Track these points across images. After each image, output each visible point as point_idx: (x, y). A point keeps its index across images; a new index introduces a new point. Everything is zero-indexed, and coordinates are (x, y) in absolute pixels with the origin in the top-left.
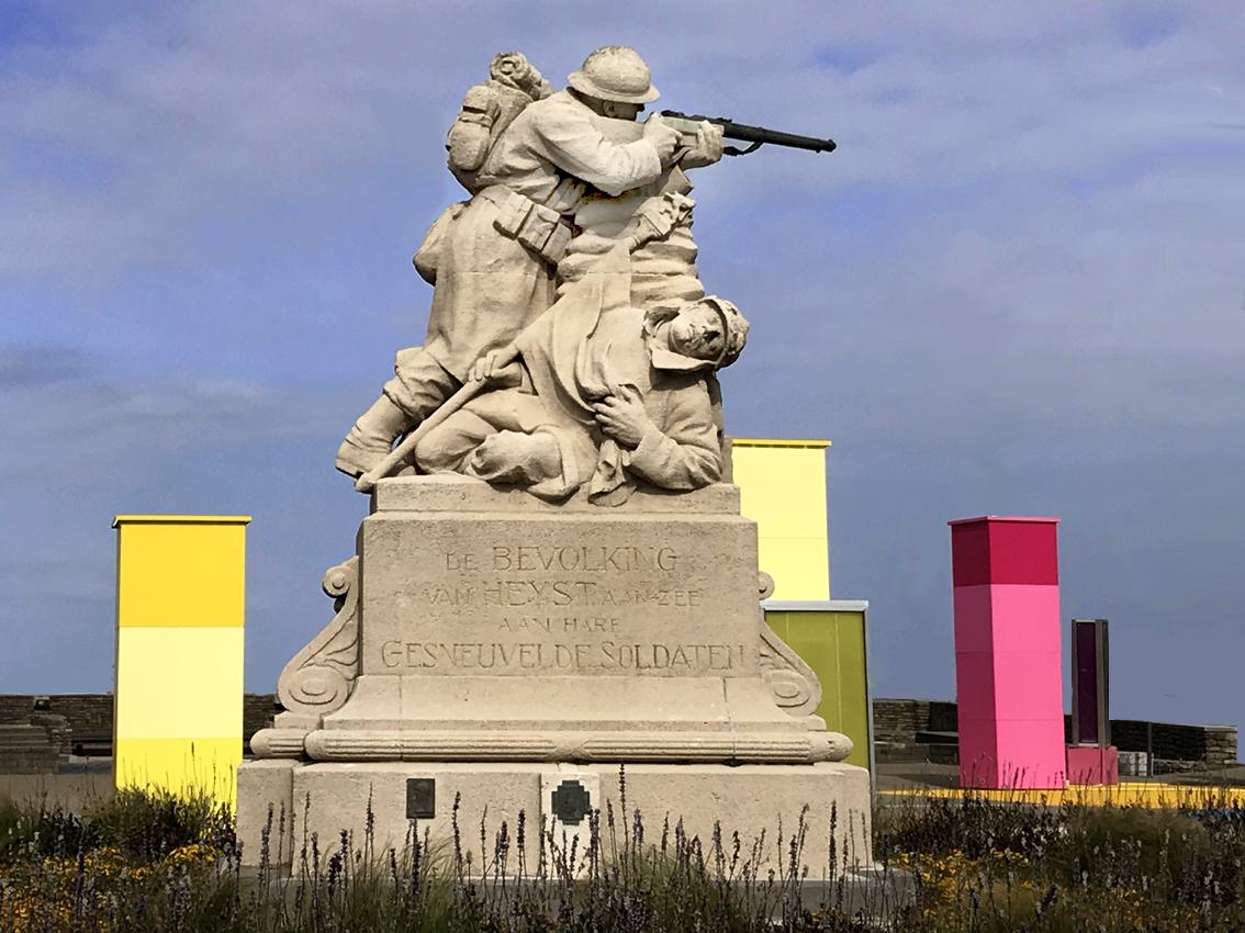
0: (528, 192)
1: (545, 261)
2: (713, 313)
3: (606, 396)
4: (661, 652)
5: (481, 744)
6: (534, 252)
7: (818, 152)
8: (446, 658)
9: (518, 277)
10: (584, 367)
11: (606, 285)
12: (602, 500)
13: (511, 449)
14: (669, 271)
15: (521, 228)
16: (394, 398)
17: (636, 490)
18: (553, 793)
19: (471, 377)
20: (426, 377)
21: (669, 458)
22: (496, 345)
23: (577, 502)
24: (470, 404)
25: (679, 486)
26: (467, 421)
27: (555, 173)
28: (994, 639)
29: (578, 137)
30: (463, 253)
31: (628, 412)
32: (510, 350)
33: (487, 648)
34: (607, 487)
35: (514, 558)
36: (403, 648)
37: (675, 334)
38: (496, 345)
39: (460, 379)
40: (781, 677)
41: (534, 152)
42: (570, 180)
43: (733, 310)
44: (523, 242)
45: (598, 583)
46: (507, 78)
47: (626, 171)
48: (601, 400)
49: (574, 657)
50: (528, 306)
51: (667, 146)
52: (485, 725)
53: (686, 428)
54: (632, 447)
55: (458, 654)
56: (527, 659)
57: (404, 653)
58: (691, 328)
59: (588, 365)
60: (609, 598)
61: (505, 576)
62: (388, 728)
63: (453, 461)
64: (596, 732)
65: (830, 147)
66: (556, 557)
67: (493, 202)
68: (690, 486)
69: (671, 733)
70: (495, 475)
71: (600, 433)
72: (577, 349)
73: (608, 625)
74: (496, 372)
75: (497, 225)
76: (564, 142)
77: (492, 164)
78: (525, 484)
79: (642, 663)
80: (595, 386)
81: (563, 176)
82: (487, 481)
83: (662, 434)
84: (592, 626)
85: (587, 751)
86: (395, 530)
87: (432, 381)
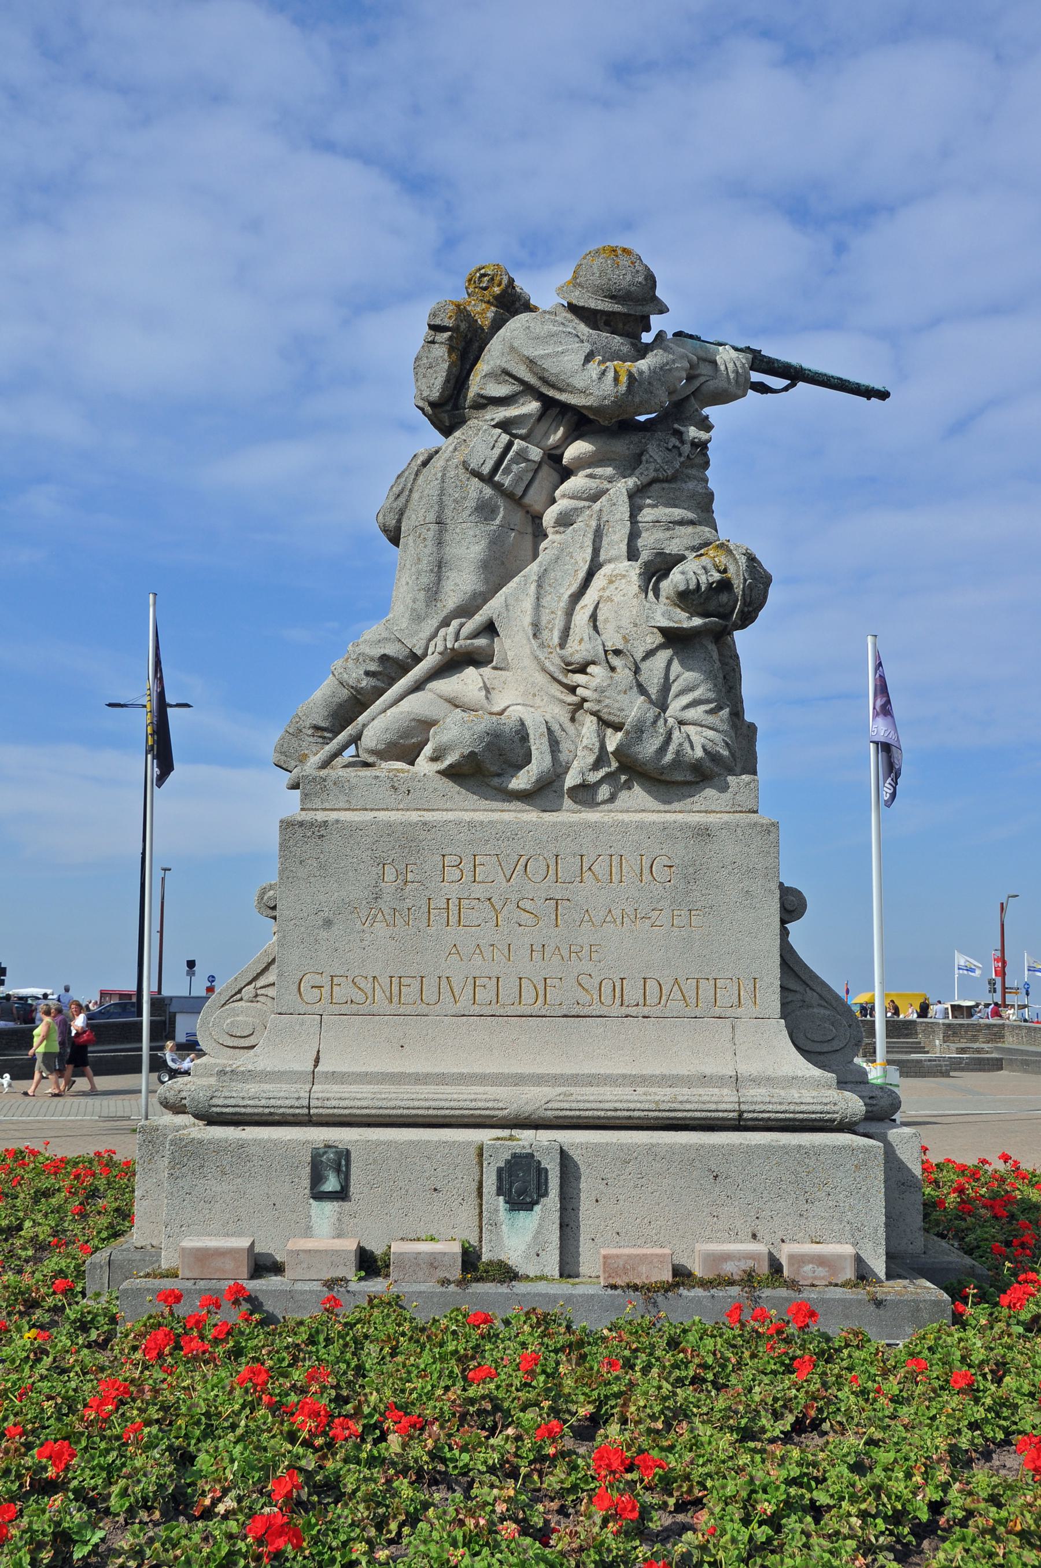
0: (504, 425)
1: (528, 512)
7: (869, 399)
22: (465, 611)
24: (432, 685)
26: (417, 705)
28: (725, 1133)
35: (467, 865)
36: (325, 981)
44: (498, 487)
48: (582, 670)
49: (541, 993)
57: (327, 988)
60: (587, 917)
63: (410, 756)
65: (883, 395)
68: (689, 778)
70: (447, 763)
75: (465, 465)
76: (542, 357)
78: (484, 776)
82: (438, 772)
84: (565, 953)
85: (549, 1113)
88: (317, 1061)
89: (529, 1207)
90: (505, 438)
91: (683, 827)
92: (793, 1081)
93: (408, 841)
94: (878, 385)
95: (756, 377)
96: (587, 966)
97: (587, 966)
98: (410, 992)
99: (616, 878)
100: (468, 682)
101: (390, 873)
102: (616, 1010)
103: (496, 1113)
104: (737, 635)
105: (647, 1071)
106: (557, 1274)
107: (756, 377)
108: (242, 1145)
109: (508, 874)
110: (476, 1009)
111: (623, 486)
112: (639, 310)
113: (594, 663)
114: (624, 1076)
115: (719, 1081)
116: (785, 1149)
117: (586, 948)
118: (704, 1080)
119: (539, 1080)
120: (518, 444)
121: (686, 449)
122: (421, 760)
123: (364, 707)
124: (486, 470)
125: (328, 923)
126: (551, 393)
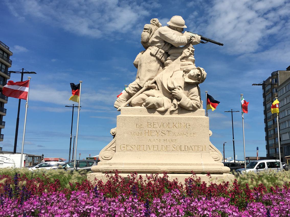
0: (158, 46)
1: (161, 62)
2: (198, 71)
3: (174, 89)
4: (186, 147)
5: (142, 169)
9: (156, 65)
10: (169, 83)
11: (175, 66)
13: (152, 100)
14: (189, 64)
16: (127, 91)
17: (181, 110)
19: (144, 86)
20: (134, 86)
21: (188, 102)
22: (151, 79)
23: (168, 112)
26: (143, 96)
27: (164, 42)
29: (169, 33)
31: (180, 92)
32: (153, 81)
33: (145, 146)
34: (174, 109)
36: (125, 146)
37: (190, 75)
38: (151, 79)
39: (142, 86)
40: (214, 154)
42: (167, 44)
43: (203, 70)
44: (157, 58)
45: (172, 131)
46: (154, 24)
47: (179, 40)
49: (166, 148)
51: (188, 38)
52: (144, 164)
53: (192, 96)
55: (139, 148)
56: (155, 149)
58: (194, 73)
59: (170, 82)
60: (174, 134)
61: (150, 129)
62: (120, 165)
63: (140, 105)
64: (170, 166)
66: (162, 125)
67: (150, 49)
69: (128, 116)
72: (168, 79)
74: (150, 85)
77: (150, 41)
79: (182, 150)
80: (172, 86)
81: (165, 42)
83: (187, 97)
84: (170, 141)
86: (125, 118)
87: (136, 87)
92: (213, 165)
94: (221, 43)
96: (174, 143)
97: (174, 143)
99: (180, 127)
103: (159, 170)
106: (21, 99)
109: (160, 126)
113: (176, 88)
117: (174, 140)
121: (190, 51)
124: (154, 54)
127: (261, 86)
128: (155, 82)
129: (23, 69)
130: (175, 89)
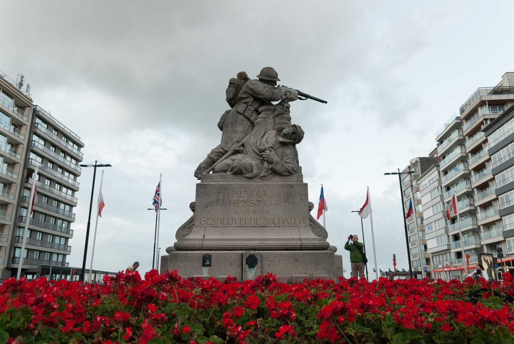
0: (246, 103)
6: (247, 118)
8: (219, 223)
12: (264, 178)
15: (244, 112)
18: (335, 250)
22: (238, 142)
25: (285, 174)
30: (371, 323)
32: (241, 143)
35: (239, 194)
36: (206, 219)
38: (238, 142)
41: (247, 92)
44: (244, 116)
48: (264, 151)
50: (246, 133)
54: (271, 163)
56: (242, 222)
65: (326, 102)
71: (263, 160)
73: (265, 213)
75: (237, 111)
80: (262, 148)
84: (261, 212)
87: (220, 152)
88: (204, 237)
89: (253, 267)
90: (246, 106)
91: (286, 185)
93: (224, 189)
94: (325, 100)
95: (299, 96)
97: (266, 216)
98: (226, 222)
100: (239, 156)
101: (221, 195)
102: (273, 225)
104: (297, 146)
105: (280, 237)
107: (299, 96)
108: (187, 254)
110: (241, 225)
111: (272, 116)
112: (274, 80)
114: (275, 239)
115: (297, 239)
116: (312, 253)
118: (293, 239)
119: (255, 240)
120: (249, 107)
121: (285, 108)
122: (228, 172)
123: (214, 163)
124: (242, 112)
125: (207, 206)
126: (256, 96)
127: (398, 175)
128: (243, 145)
129: (96, 161)
130: (266, 151)
